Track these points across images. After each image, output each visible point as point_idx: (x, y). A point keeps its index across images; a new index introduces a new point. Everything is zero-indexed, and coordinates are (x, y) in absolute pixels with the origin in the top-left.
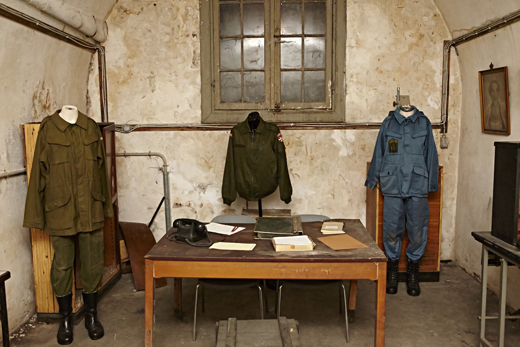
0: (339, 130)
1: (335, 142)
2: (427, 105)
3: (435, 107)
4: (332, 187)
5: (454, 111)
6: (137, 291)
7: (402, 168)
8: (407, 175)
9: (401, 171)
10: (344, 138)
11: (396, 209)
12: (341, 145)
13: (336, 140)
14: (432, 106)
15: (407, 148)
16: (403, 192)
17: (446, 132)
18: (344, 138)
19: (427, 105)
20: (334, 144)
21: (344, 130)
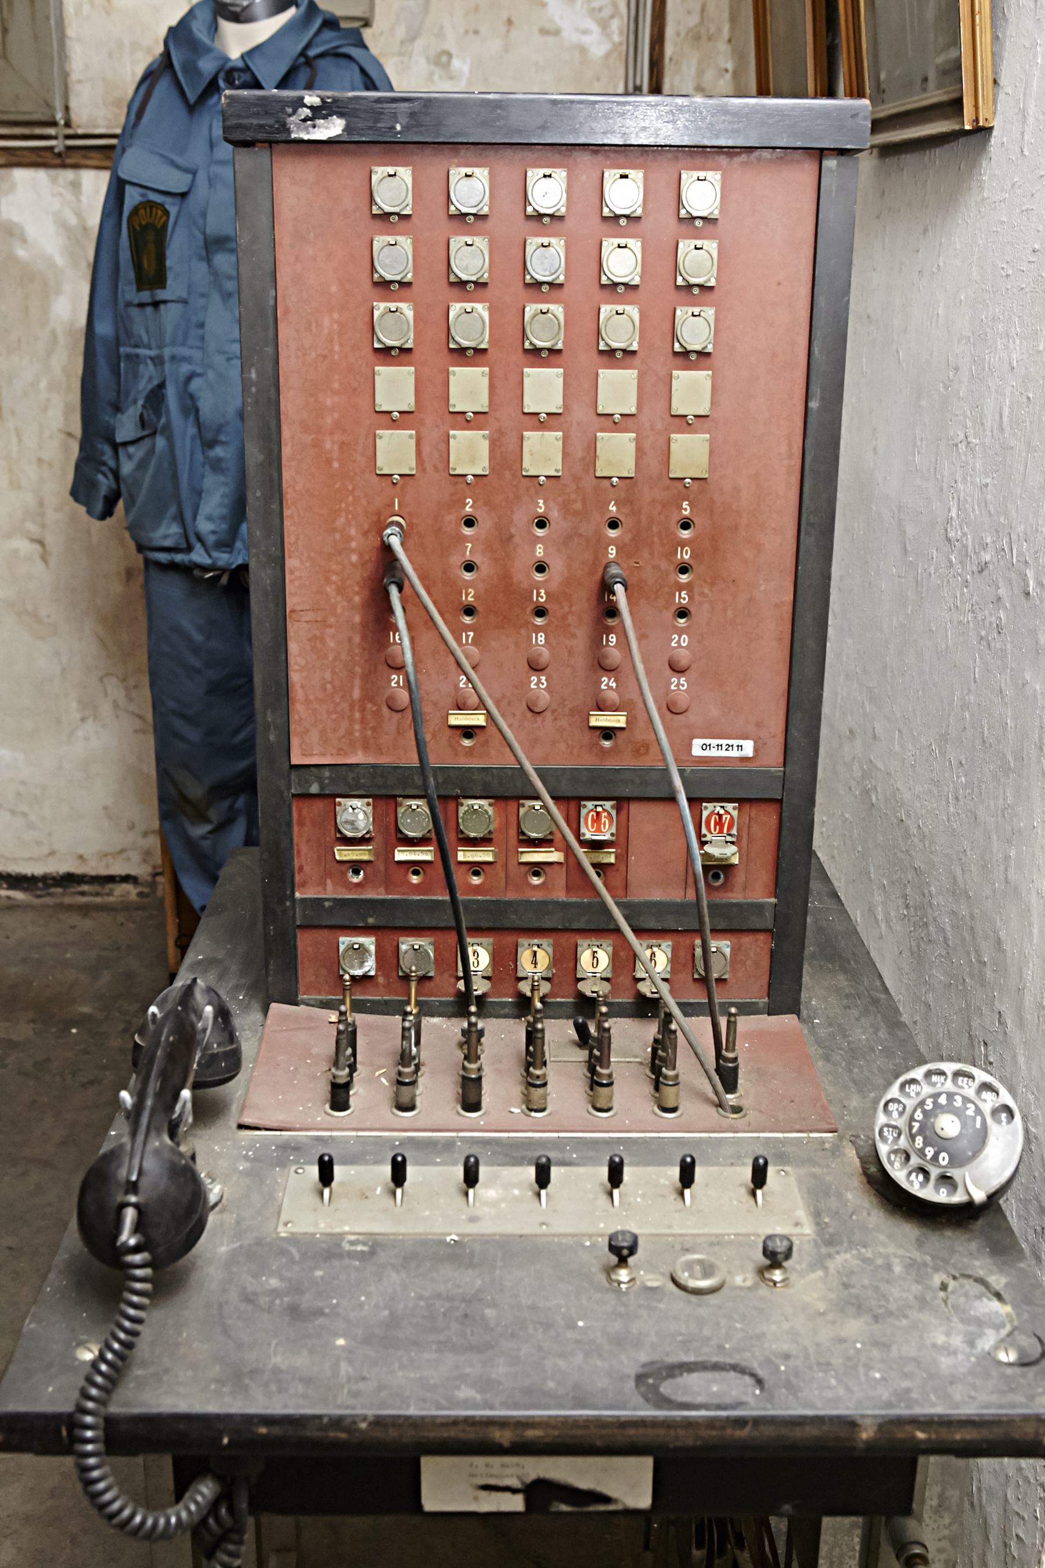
0: (41, 175)
1: (24, 240)
2: (544, 32)
3: (586, 39)
4: (29, 499)
5: (701, 73)
6: (538, 414)
7: (195, 384)
8: (220, 428)
9: (191, 407)
10: (73, 221)
11: (188, 639)
12: (60, 260)
13: (32, 231)
14: (570, 35)
15: (223, 261)
16: (200, 539)
17: (886, 151)
18: (73, 221)
19: (544, 32)
20: (21, 253)
21: (69, 174)
